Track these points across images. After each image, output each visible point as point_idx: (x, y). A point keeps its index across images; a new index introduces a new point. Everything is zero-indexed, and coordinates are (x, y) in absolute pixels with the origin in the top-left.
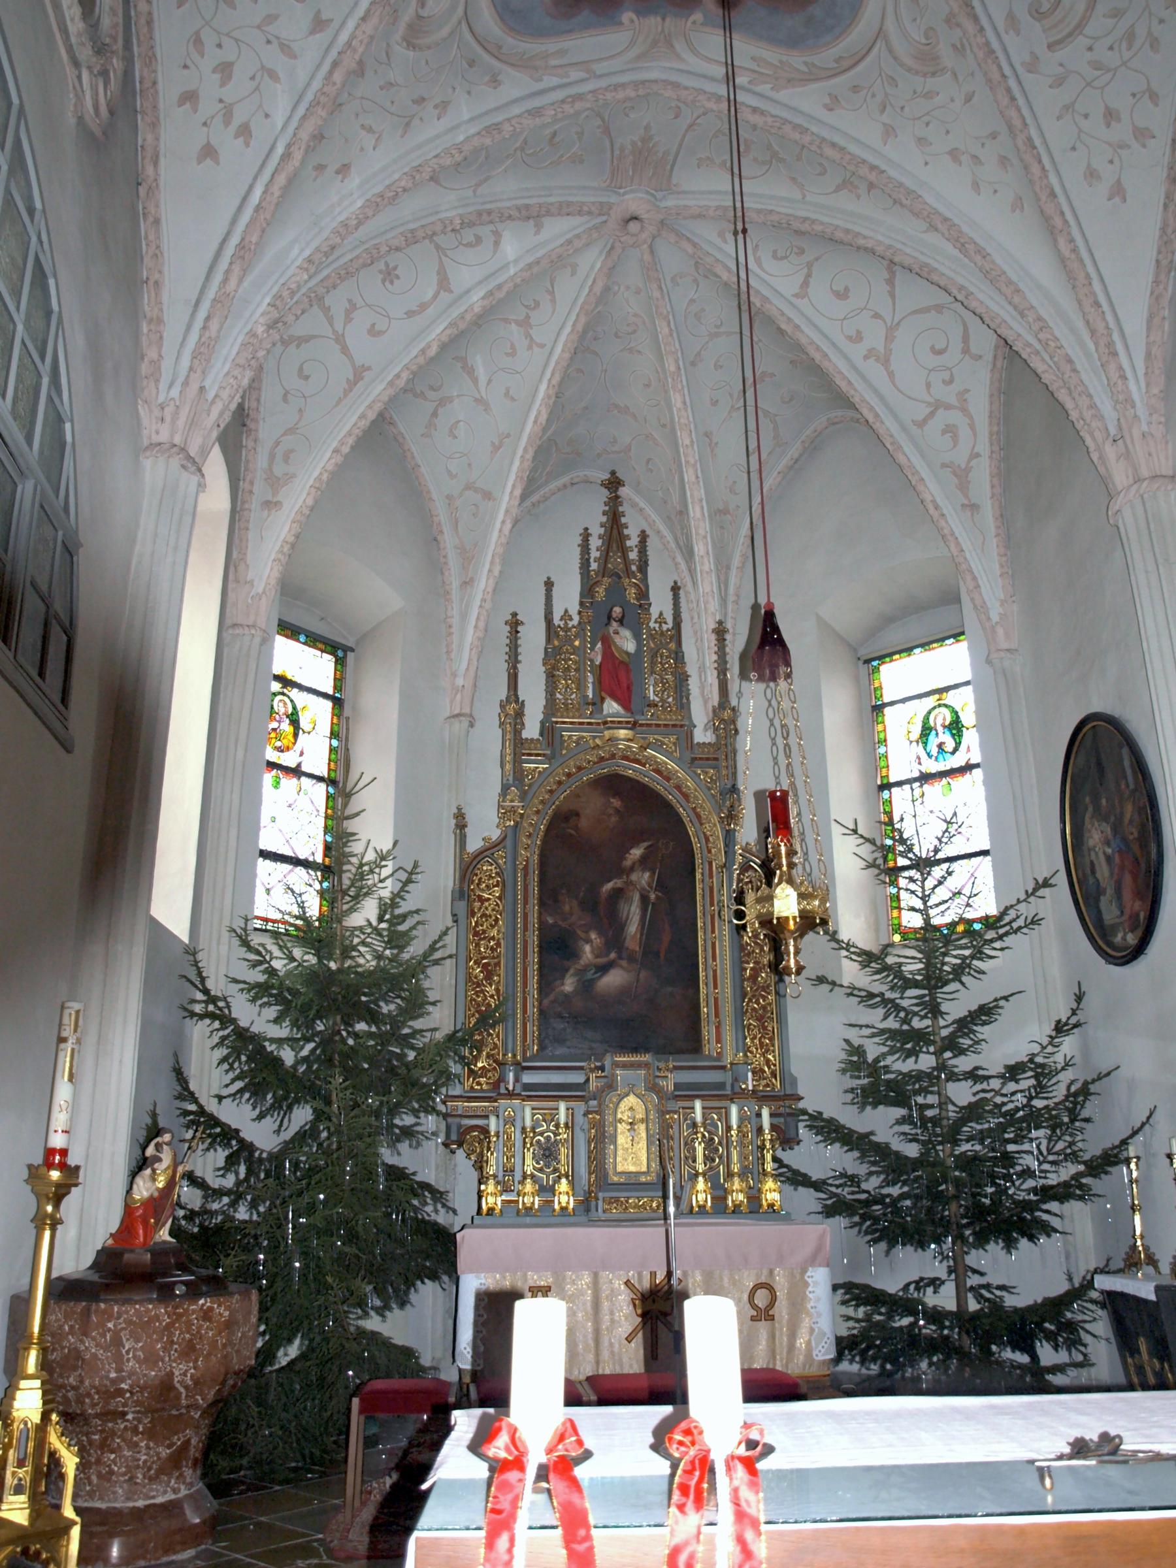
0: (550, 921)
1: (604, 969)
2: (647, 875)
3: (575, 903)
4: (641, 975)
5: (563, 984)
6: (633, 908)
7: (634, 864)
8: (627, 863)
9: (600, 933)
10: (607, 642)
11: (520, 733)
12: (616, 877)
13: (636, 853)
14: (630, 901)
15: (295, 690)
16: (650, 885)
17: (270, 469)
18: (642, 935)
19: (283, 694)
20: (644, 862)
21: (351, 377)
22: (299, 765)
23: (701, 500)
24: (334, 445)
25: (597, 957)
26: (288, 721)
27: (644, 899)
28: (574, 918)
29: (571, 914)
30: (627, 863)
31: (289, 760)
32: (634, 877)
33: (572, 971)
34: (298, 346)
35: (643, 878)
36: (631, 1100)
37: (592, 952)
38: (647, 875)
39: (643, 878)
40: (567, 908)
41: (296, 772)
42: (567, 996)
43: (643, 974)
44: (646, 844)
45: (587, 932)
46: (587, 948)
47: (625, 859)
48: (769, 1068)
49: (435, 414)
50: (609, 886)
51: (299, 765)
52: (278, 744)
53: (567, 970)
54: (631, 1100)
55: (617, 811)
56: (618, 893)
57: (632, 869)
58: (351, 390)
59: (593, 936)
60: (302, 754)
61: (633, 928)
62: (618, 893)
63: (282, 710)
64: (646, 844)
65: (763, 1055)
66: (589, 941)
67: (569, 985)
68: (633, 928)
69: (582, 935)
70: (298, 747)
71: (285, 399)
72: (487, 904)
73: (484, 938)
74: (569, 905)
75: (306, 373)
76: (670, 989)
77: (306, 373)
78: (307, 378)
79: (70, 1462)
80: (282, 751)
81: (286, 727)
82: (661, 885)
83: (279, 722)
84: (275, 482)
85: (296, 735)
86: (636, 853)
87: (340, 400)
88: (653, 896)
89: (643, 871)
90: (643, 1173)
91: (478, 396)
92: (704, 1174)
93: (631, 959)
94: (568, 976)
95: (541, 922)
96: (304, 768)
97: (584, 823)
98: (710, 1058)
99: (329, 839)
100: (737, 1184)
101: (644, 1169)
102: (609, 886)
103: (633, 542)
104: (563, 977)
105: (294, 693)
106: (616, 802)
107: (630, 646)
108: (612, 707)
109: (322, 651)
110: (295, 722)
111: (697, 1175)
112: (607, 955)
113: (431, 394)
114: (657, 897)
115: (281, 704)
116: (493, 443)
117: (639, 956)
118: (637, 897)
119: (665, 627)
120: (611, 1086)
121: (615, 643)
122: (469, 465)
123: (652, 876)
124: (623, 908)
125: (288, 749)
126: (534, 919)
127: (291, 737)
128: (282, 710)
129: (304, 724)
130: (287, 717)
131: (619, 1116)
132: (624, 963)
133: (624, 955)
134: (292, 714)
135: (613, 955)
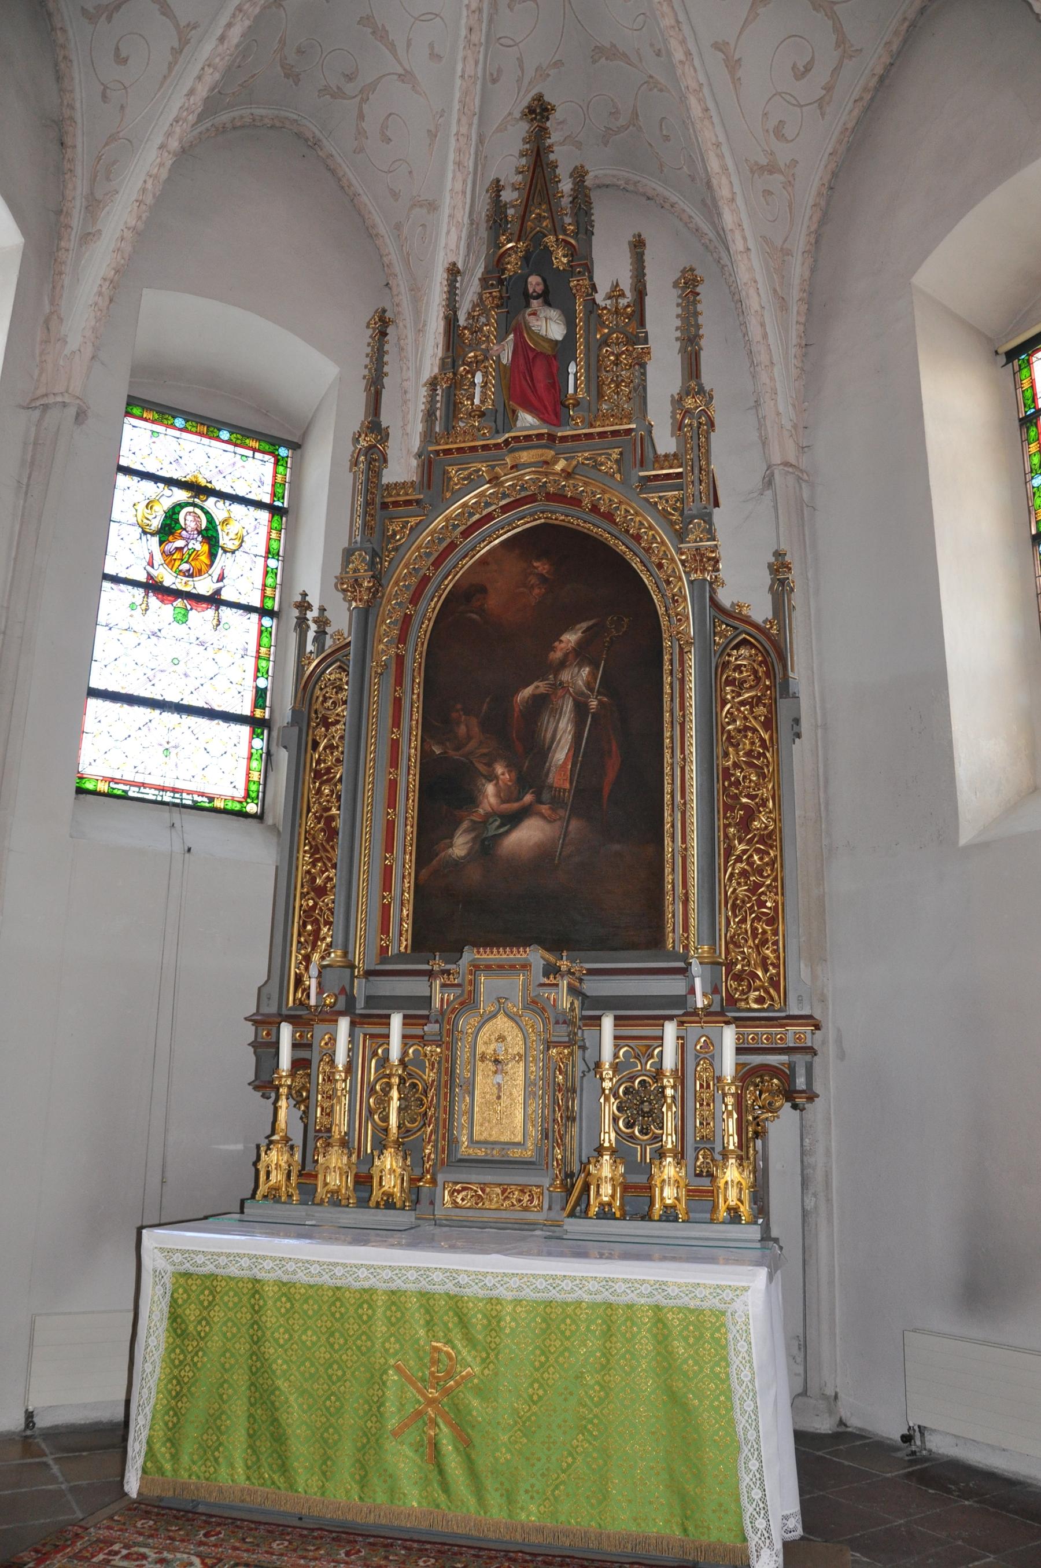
0: (437, 750)
1: (513, 820)
2: (585, 671)
3: (474, 721)
4: (571, 828)
5: (451, 846)
6: (562, 725)
7: (566, 655)
8: (557, 655)
9: (509, 766)
10: (520, 331)
11: (378, 475)
12: (537, 679)
13: (571, 638)
14: (556, 713)
15: (212, 500)
16: (589, 686)
17: (92, 194)
18: (574, 765)
19: (195, 505)
20: (581, 653)
21: (176, 45)
22: (218, 592)
23: (718, 145)
24: (159, 140)
25: (503, 802)
26: (200, 538)
27: (581, 709)
28: (472, 745)
29: (469, 738)
30: (557, 655)
31: (204, 586)
32: (565, 676)
33: (465, 825)
34: (109, 19)
35: (579, 676)
36: (501, 1023)
37: (498, 795)
38: (585, 671)
39: (579, 676)
40: (462, 730)
41: (215, 600)
42: (457, 865)
43: (574, 824)
44: (584, 625)
45: (490, 765)
46: (490, 789)
47: (553, 649)
48: (766, 971)
49: (361, 117)
50: (528, 691)
51: (218, 592)
52: (185, 567)
53: (457, 823)
54: (501, 1023)
55: (543, 579)
56: (540, 702)
57: (563, 664)
58: (176, 63)
59: (499, 769)
60: (221, 578)
61: (561, 755)
62: (540, 702)
63: (191, 525)
64: (584, 625)
65: (758, 948)
66: (492, 777)
67: (460, 846)
68: (561, 755)
69: (482, 768)
70: (216, 571)
71: (104, 97)
72: (333, 729)
73: (329, 781)
74: (467, 727)
75: (123, 55)
76: (617, 847)
77: (123, 55)
78: (125, 61)
79: (449, 1350)
80: (191, 576)
81: (198, 545)
82: (608, 686)
83: (187, 540)
84: (94, 205)
85: (212, 556)
86: (571, 638)
87: (165, 77)
88: (594, 704)
89: (580, 666)
90: (518, 1144)
91: (401, 71)
92: (613, 1152)
93: (556, 802)
94: (459, 832)
95: (425, 755)
96: (225, 595)
97: (493, 602)
98: (674, 956)
99: (262, 683)
100: (669, 1169)
101: (519, 1138)
102: (528, 691)
103: (566, 186)
104: (451, 836)
105: (210, 503)
106: (541, 567)
107: (556, 331)
108: (527, 420)
109: (254, 450)
110: (210, 537)
111: (600, 1150)
112: (519, 799)
113: (349, 88)
114: (600, 702)
115: (190, 518)
116: (429, 131)
117: (569, 798)
118: (568, 706)
119: (623, 302)
120: (469, 1002)
121: (528, 328)
122: (410, 172)
123: (593, 674)
124: (547, 724)
125: (200, 573)
126: (411, 750)
127: (204, 558)
128: (191, 525)
129: (224, 540)
130: (199, 533)
131: (481, 1048)
132: (544, 809)
133: (546, 796)
134: (207, 529)
135: (528, 798)
